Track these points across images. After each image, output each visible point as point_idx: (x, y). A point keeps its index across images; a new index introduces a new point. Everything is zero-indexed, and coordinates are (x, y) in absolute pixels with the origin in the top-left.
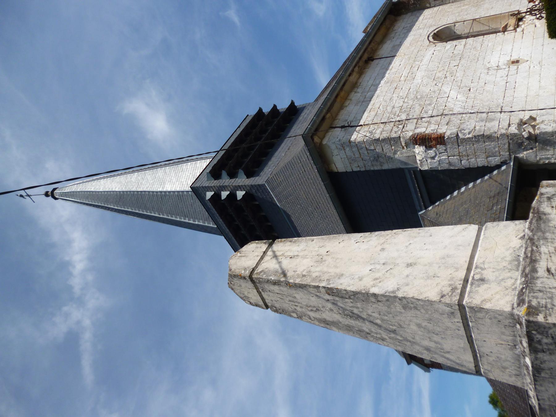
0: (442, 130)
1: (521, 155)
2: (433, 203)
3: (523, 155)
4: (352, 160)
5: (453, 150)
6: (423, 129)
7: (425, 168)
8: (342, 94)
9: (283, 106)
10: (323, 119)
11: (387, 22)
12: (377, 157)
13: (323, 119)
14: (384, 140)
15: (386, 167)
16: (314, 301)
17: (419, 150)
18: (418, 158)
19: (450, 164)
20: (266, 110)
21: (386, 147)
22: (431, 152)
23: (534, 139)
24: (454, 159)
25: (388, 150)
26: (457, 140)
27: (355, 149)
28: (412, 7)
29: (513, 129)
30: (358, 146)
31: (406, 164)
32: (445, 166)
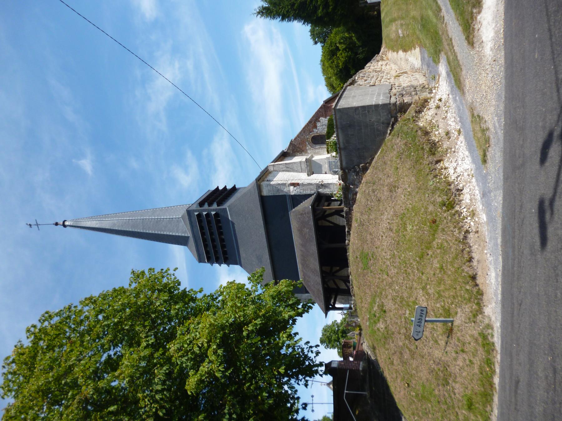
0: (299, 182)
1: (319, 190)
2: (294, 208)
3: (320, 190)
4: (269, 191)
5: (301, 188)
6: (293, 182)
7: (293, 194)
8: (266, 174)
9: (229, 187)
10: (261, 178)
11: (281, 158)
12: (278, 190)
13: (261, 178)
14: (281, 184)
15: (280, 194)
16: (283, 167)
17: (292, 188)
18: (291, 190)
19: (300, 192)
20: (221, 188)
21: (282, 186)
22: (295, 188)
23: (322, 185)
24: (302, 191)
25: (282, 187)
26: (303, 185)
27: (271, 187)
28: (232, 335)
29: (318, 183)
30: (272, 185)
31: (287, 193)
32: (299, 193)
